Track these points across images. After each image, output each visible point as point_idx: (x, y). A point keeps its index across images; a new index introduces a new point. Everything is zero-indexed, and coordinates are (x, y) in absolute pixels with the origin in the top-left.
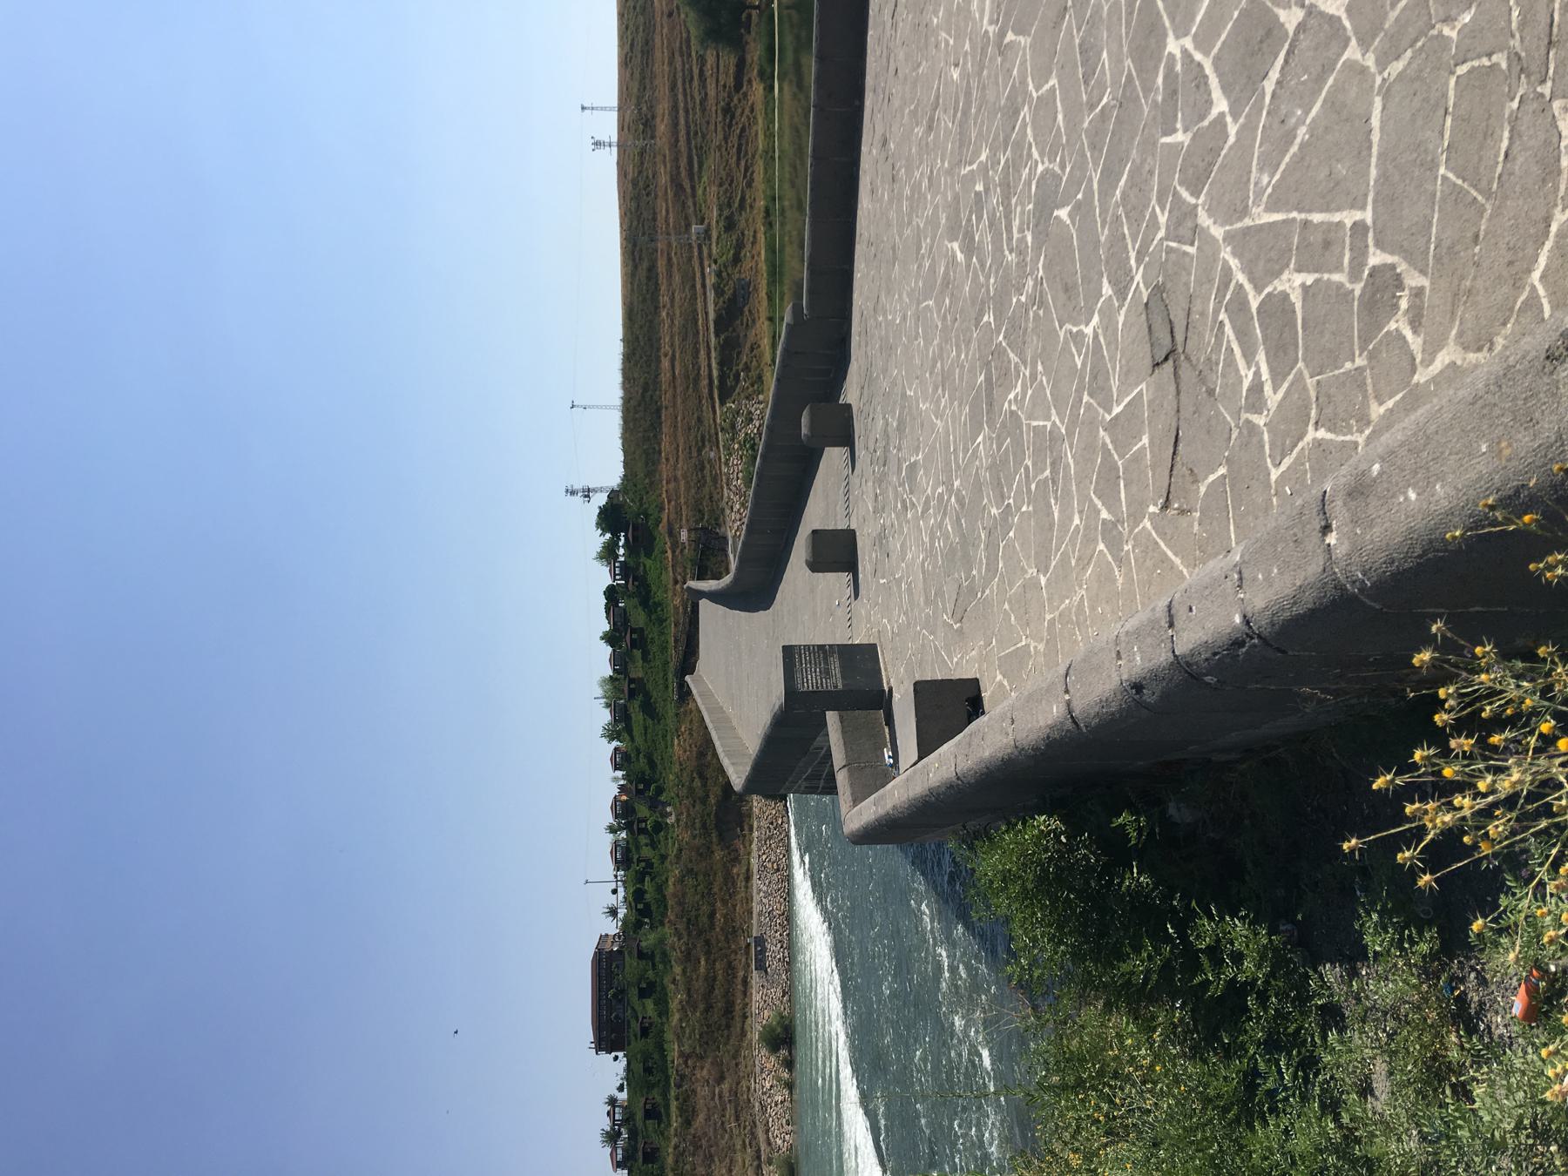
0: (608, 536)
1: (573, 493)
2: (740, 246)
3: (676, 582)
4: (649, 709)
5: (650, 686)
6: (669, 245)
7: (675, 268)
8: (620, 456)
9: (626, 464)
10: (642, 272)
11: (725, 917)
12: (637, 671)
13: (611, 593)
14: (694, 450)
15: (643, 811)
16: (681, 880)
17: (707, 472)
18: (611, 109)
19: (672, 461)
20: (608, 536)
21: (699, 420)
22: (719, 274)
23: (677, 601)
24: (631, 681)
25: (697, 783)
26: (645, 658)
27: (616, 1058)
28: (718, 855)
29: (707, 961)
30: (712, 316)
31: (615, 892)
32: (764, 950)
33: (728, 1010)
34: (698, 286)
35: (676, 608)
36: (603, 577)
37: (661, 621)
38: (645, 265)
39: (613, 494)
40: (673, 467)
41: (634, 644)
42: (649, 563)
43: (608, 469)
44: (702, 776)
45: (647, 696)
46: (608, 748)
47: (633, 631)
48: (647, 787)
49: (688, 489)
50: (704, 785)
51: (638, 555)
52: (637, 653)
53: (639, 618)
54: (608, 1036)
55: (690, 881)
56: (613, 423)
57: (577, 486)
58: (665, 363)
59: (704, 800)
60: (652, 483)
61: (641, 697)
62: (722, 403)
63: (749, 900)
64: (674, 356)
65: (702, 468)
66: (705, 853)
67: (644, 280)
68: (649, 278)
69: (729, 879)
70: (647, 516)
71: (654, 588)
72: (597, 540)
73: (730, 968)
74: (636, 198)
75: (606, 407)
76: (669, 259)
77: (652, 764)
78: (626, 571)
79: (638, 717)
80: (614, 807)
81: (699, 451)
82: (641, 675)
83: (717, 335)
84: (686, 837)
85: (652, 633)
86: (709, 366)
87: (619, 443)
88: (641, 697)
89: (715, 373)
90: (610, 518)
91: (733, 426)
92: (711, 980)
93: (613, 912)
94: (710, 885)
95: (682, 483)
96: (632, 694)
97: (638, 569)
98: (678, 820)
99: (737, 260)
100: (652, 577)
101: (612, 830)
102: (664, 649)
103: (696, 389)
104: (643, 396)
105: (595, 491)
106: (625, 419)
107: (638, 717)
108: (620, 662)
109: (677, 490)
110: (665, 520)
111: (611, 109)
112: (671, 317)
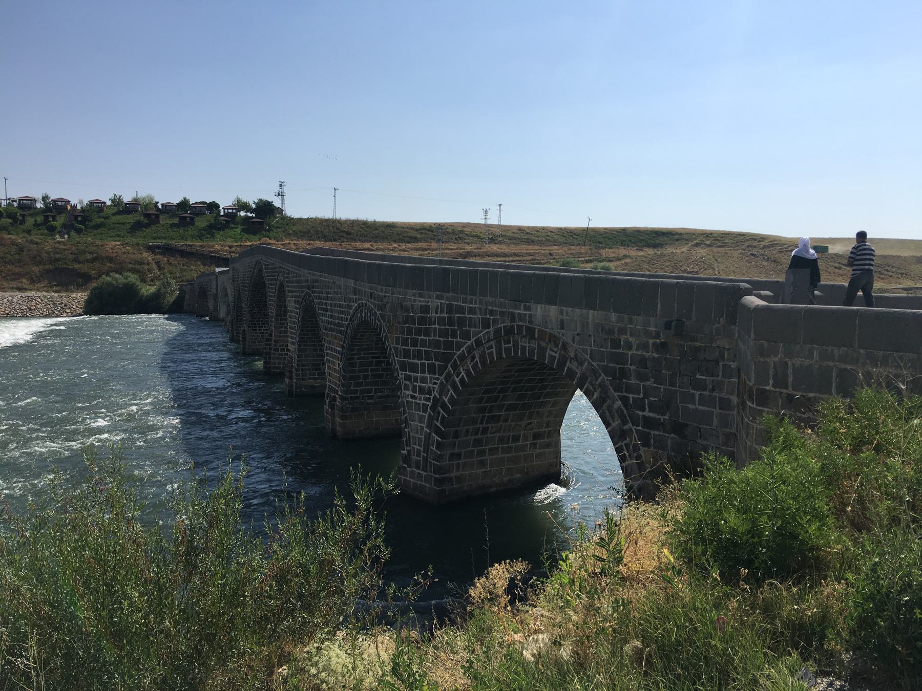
0: (254, 206)
1: (281, 186)
3: (230, 247)
4: (137, 227)
5: (154, 227)
7: (421, 252)
8: (305, 217)
9: (300, 219)
10: (414, 234)
12: (164, 220)
13: (213, 206)
15: (61, 220)
16: (13, 243)
18: (335, 212)
20: (254, 206)
23: (218, 247)
24: (157, 216)
25: (89, 256)
26: (173, 225)
28: (36, 269)
35: (213, 246)
36: (225, 201)
37: (200, 237)
38: (419, 236)
39: (280, 211)
42: (239, 230)
43: (296, 208)
44: (94, 260)
45: (148, 226)
47: (192, 219)
50: (88, 261)
51: (243, 224)
52: (176, 221)
53: (201, 223)
55: (13, 249)
56: (325, 212)
57: (285, 189)
58: (367, 245)
59: (76, 260)
60: (290, 234)
61: (146, 221)
64: (372, 250)
66: (36, 259)
67: (410, 234)
68: (411, 237)
69: (17, 276)
70: (269, 231)
71: (222, 233)
72: (251, 199)
74: (454, 232)
75: (500, 217)
76: (426, 250)
77: (97, 227)
79: (131, 219)
80: (61, 200)
85: (191, 231)
87: (313, 215)
88: (146, 221)
90: (265, 209)
97: (233, 223)
98: (59, 242)
100: (229, 232)
101: (45, 198)
102: (183, 238)
105: (282, 199)
106: (327, 220)
107: (131, 219)
108: (168, 209)
110: (270, 241)
111: (335, 212)
112: (393, 250)
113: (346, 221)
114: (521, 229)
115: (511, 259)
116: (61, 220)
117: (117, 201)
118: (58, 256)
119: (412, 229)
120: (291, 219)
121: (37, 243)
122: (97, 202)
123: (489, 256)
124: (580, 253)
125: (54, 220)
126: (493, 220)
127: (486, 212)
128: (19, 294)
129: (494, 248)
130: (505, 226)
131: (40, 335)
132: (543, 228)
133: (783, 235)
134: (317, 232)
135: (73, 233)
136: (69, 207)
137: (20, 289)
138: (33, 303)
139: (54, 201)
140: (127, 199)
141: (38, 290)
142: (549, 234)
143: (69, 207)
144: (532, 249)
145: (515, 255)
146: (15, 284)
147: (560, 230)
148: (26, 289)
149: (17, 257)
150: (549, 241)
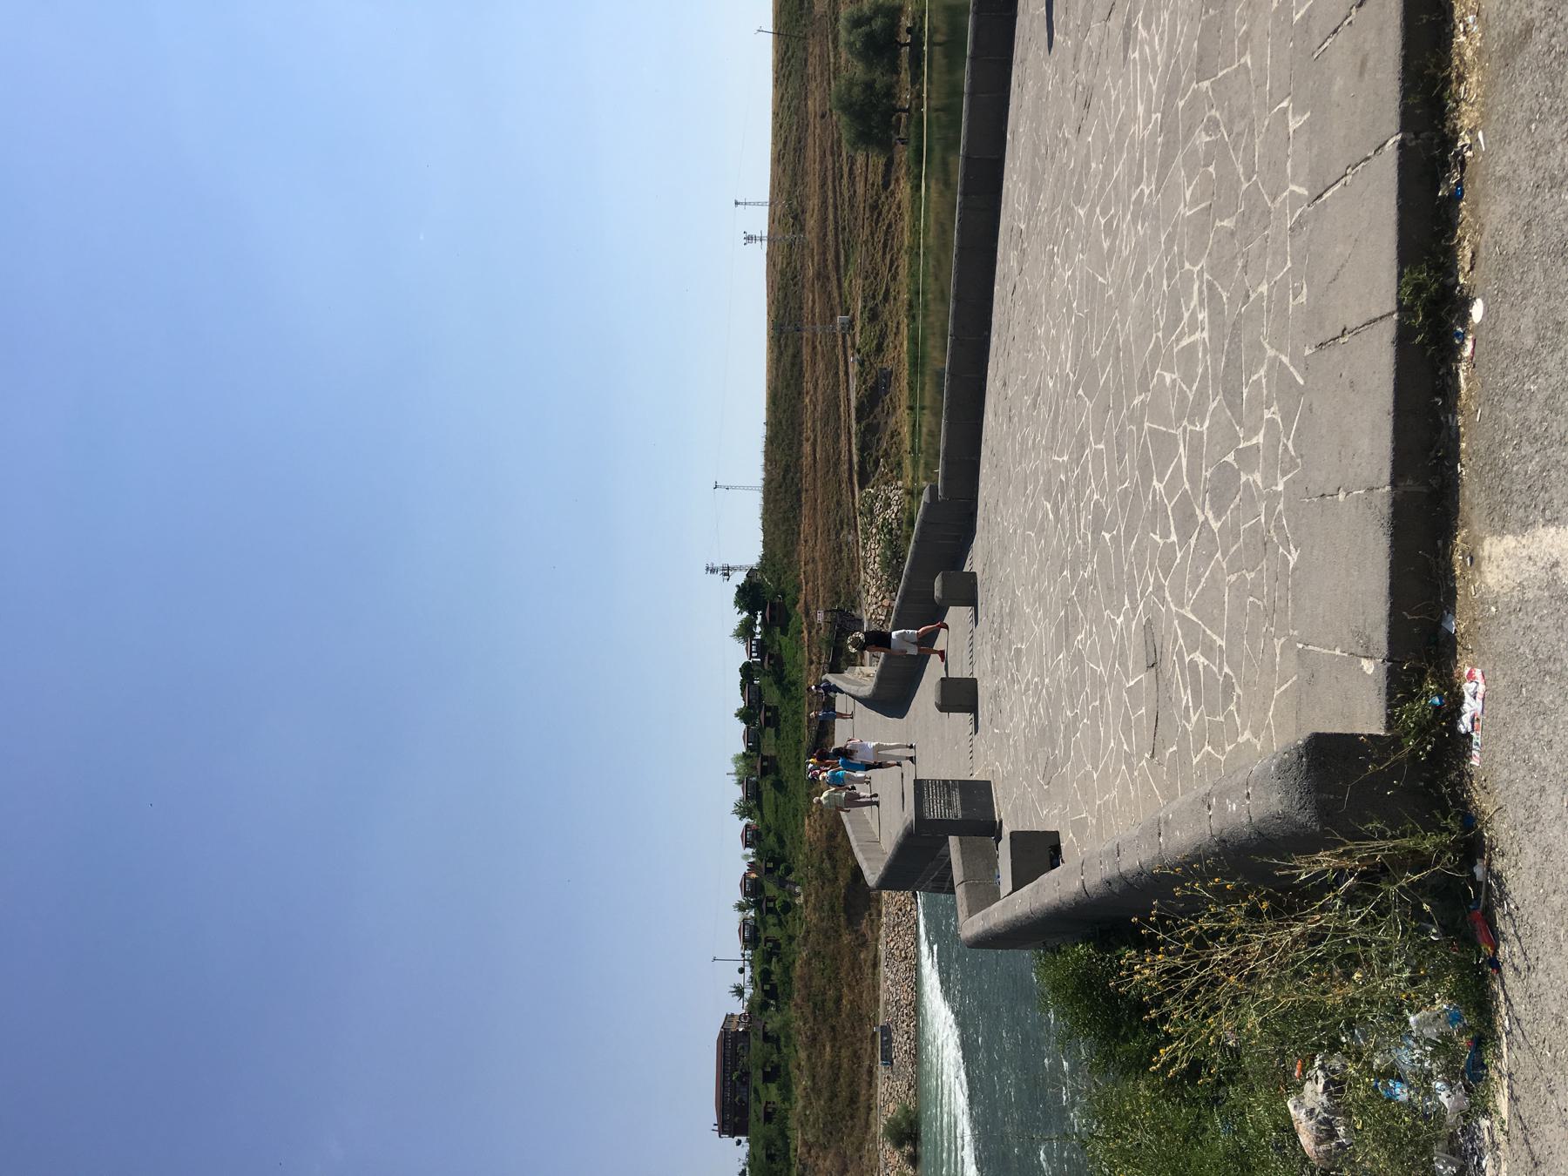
0: (745, 614)
1: (713, 571)
2: (883, 336)
3: (811, 662)
5: (782, 765)
6: (815, 334)
7: (819, 357)
9: (765, 543)
10: (787, 359)
11: (851, 1002)
12: (769, 748)
13: (747, 670)
14: (833, 533)
15: (771, 889)
16: (808, 963)
17: (844, 554)
19: (810, 544)
20: (745, 614)
21: (839, 503)
22: (862, 364)
25: (827, 865)
26: (777, 736)
27: (739, 1143)
28: (846, 938)
29: (833, 1047)
30: (853, 403)
31: (742, 971)
32: (890, 1041)
33: (853, 1100)
34: (841, 374)
36: (739, 654)
38: (790, 351)
39: (751, 573)
40: (811, 549)
41: (768, 722)
42: (785, 640)
43: (748, 549)
44: (831, 857)
45: (777, 771)
46: (739, 825)
47: (768, 709)
48: (776, 867)
49: (826, 570)
50: (834, 867)
52: (770, 731)
53: (773, 696)
54: (732, 1120)
57: (718, 565)
58: (807, 448)
62: (862, 488)
63: (875, 987)
65: (840, 551)
67: (788, 366)
68: (793, 365)
69: (856, 965)
72: (736, 617)
73: (856, 1057)
74: (784, 288)
75: (757, 204)
76: (814, 348)
77: (781, 841)
78: (762, 648)
79: (768, 792)
81: (838, 534)
82: (773, 753)
83: (858, 421)
84: (814, 918)
85: (785, 713)
86: (850, 451)
88: (772, 777)
89: (855, 459)
90: (749, 596)
91: (871, 511)
92: (836, 1068)
93: (739, 992)
94: (836, 971)
95: (820, 564)
96: (764, 772)
98: (806, 901)
99: (879, 348)
102: (797, 728)
103: (836, 473)
104: (784, 478)
105: (734, 569)
106: (766, 500)
107: (768, 792)
109: (815, 571)
110: (802, 601)
113: (766, 470)
114: (778, 159)
115: (830, 194)
116: (771, 889)
117: (743, 811)
118: (826, 907)
119: (778, 360)
120: (764, 557)
121: (808, 932)
122: (742, 930)
123: (825, 235)
124: (821, 56)
125: (773, 900)
126: (759, 221)
127: (749, 238)
128: (883, 969)
129: (811, 223)
130: (772, 193)
131: (947, 994)
132: (776, 114)
133: (764, 406)
134: (786, 520)
135: (791, 877)
136: (754, 875)
137: (875, 965)
138: (897, 953)
139: (746, 894)
140: (737, 793)
141: (877, 940)
142: (785, 103)
143: (754, 875)
144: (813, 152)
145: (823, 185)
146: (868, 970)
147: (778, 81)
148: (876, 956)
149: (828, 961)
150: (798, 109)
